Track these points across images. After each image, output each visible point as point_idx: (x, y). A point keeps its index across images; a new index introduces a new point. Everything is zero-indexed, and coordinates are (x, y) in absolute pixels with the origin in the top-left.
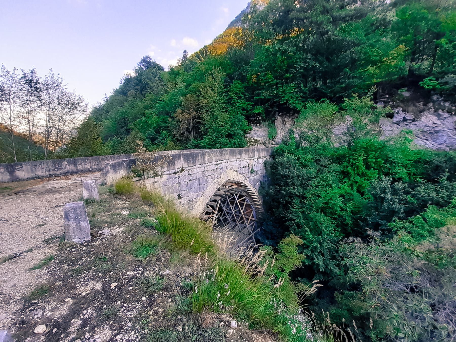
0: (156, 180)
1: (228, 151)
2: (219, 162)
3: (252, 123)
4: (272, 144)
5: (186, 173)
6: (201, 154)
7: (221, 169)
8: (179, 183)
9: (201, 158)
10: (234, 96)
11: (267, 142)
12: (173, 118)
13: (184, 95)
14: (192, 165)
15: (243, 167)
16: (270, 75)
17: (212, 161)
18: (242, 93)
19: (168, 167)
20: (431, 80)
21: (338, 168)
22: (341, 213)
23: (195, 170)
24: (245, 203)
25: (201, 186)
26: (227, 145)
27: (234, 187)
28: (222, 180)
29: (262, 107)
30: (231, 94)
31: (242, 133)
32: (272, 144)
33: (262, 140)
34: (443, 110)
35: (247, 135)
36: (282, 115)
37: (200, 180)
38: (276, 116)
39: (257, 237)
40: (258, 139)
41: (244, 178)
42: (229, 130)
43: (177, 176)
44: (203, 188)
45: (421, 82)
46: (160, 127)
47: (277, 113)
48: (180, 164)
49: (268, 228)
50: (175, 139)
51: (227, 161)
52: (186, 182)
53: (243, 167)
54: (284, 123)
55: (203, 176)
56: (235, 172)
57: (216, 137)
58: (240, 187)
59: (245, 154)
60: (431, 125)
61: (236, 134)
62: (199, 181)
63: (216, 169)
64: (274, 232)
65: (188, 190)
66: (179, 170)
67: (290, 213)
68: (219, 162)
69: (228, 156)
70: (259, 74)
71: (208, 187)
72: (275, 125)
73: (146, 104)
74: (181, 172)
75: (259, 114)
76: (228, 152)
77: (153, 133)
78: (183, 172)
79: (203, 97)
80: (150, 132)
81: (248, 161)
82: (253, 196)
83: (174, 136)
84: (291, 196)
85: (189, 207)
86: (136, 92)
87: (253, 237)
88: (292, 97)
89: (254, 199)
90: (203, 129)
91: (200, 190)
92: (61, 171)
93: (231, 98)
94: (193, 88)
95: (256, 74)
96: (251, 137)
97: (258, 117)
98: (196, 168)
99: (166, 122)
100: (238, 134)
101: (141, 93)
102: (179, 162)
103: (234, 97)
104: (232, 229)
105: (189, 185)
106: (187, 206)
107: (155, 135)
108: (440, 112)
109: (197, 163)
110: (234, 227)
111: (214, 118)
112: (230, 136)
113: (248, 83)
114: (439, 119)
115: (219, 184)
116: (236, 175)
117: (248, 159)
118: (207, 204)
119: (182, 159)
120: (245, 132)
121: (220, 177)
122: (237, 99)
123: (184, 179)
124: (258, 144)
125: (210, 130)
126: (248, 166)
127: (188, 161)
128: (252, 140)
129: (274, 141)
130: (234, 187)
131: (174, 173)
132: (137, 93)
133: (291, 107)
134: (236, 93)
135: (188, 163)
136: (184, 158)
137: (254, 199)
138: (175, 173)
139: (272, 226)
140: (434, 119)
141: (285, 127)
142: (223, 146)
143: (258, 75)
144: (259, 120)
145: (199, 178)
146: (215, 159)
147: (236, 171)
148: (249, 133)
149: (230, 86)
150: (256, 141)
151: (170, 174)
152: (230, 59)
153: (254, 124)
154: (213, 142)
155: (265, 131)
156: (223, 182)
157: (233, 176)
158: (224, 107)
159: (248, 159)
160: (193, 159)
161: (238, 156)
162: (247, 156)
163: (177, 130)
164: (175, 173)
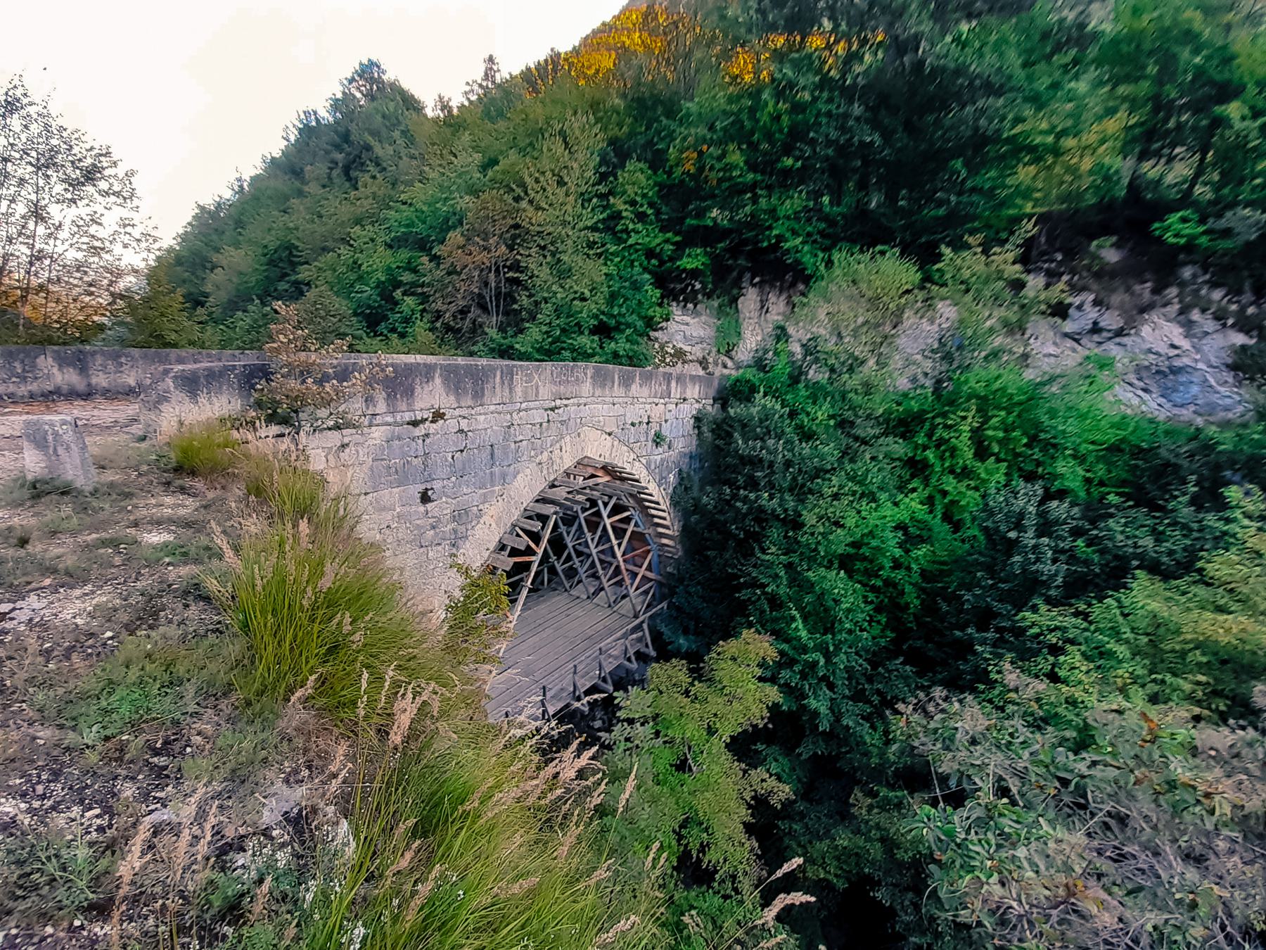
2: (558, 402)
4: (725, 366)
5: (452, 425)
11: (711, 360)
12: (435, 258)
13: (474, 191)
14: (470, 403)
18: (651, 205)
19: (391, 397)
20: (1184, 220)
21: (899, 448)
24: (631, 528)
25: (496, 470)
26: (593, 355)
27: (599, 480)
29: (706, 253)
30: (618, 203)
32: (725, 366)
33: (697, 351)
34: (1203, 311)
40: (687, 348)
41: (633, 456)
42: (603, 313)
44: (504, 476)
45: (1157, 225)
46: (398, 285)
47: (748, 276)
48: (432, 395)
51: (582, 401)
53: (633, 424)
54: (763, 307)
57: (563, 331)
60: (1163, 348)
62: (492, 455)
65: (453, 479)
68: (558, 402)
69: (587, 388)
75: (695, 274)
78: (441, 422)
81: (648, 407)
82: (653, 512)
84: (761, 516)
85: (455, 531)
87: (645, 626)
90: (525, 301)
92: (34, 387)
93: (617, 216)
96: (666, 339)
99: (415, 271)
100: (628, 326)
102: (427, 388)
103: (624, 214)
105: (459, 465)
108: (1195, 315)
109: (486, 399)
110: (596, 593)
111: (563, 273)
112: (603, 330)
113: (670, 173)
119: (438, 381)
120: (650, 324)
124: (684, 362)
125: (547, 308)
127: (457, 389)
128: (669, 350)
129: (731, 358)
130: (599, 480)
131: (408, 424)
134: (633, 203)
136: (446, 380)
138: (415, 423)
140: (1175, 333)
142: (581, 355)
143: (701, 153)
144: (695, 292)
146: (545, 391)
147: (610, 434)
148: (661, 329)
150: (679, 354)
151: (396, 424)
152: (624, 96)
153: (678, 302)
156: (568, 462)
157: (599, 448)
161: (618, 390)
162: (645, 391)
163: (449, 299)
164: (415, 423)
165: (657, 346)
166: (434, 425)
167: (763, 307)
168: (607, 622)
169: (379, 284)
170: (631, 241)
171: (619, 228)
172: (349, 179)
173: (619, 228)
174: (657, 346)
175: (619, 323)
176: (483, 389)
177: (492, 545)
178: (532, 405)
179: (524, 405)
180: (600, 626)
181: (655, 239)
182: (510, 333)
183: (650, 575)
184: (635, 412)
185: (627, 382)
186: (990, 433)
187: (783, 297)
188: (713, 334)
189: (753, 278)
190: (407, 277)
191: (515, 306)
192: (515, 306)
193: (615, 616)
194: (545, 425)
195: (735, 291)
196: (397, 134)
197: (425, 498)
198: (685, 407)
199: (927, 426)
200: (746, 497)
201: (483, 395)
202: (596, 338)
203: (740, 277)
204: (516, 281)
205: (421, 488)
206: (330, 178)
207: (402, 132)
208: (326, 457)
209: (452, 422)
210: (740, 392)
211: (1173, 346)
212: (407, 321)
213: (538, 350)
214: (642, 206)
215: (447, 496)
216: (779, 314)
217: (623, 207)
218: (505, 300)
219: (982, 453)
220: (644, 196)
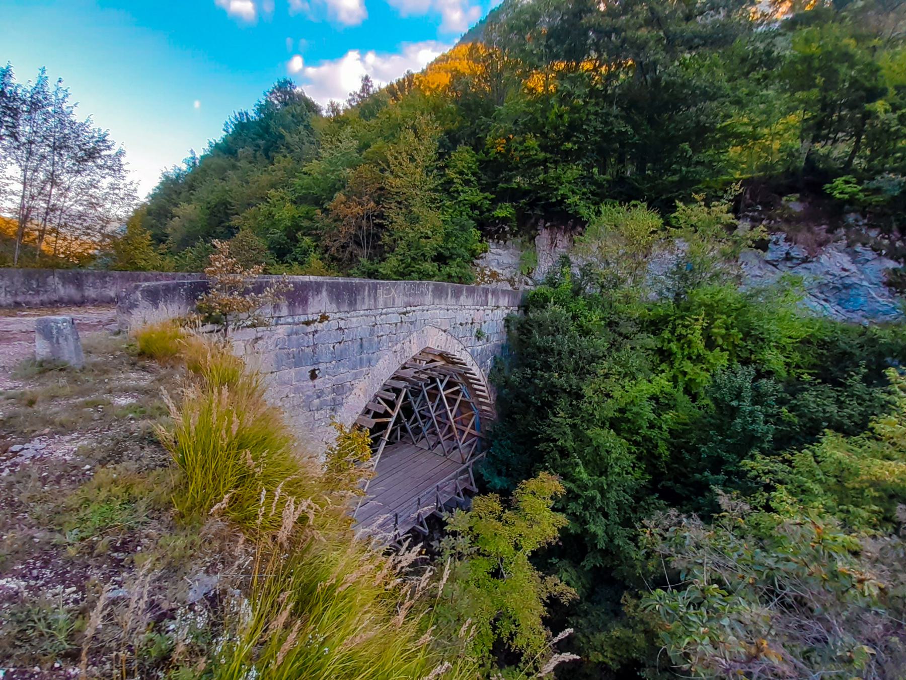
0: (259, 335)
2: (408, 309)
4: (527, 284)
5: (334, 324)
7: (412, 323)
8: (315, 345)
9: (369, 295)
11: (516, 279)
12: (325, 211)
14: (346, 309)
15: (461, 324)
18: (474, 174)
19: (291, 305)
20: (847, 182)
23: (354, 320)
24: (460, 398)
25: (364, 356)
27: (437, 364)
30: (451, 173)
31: (467, 255)
32: (527, 284)
33: (507, 273)
34: (864, 245)
35: (478, 261)
40: (500, 271)
42: (441, 247)
43: (311, 328)
45: (828, 186)
46: (299, 228)
48: (320, 304)
51: (426, 307)
53: (461, 324)
54: (553, 243)
55: (372, 333)
57: (413, 259)
60: (837, 272)
65: (334, 362)
68: (408, 309)
69: (429, 298)
70: (511, 136)
75: (505, 220)
78: (326, 322)
81: (472, 312)
87: (470, 469)
88: (573, 192)
90: (387, 239)
93: (450, 182)
94: (373, 153)
99: (311, 219)
100: (459, 256)
102: (317, 299)
105: (338, 352)
107: (286, 243)
108: (859, 248)
109: (358, 306)
111: (414, 220)
112: (441, 259)
113: (487, 153)
114: (854, 262)
117: (473, 307)
120: (474, 254)
121: (408, 339)
125: (402, 244)
128: (487, 272)
130: (437, 364)
131: (303, 323)
132: (258, 154)
134: (461, 173)
138: (307, 323)
143: (508, 140)
147: (445, 331)
148: (482, 258)
149: (450, 157)
150: (494, 275)
153: (493, 239)
156: (415, 351)
157: (437, 341)
158: (436, 199)
162: (470, 301)
164: (307, 323)
165: (478, 269)
166: (321, 325)
169: (286, 228)
172: (268, 157)
174: (478, 269)
175: (452, 254)
177: (360, 411)
178: (389, 310)
179: (384, 311)
182: (376, 260)
185: (457, 294)
187: (568, 235)
189: (545, 223)
196: (301, 127)
197: (313, 376)
202: (436, 264)
203: (536, 223)
206: (255, 157)
211: (844, 270)
212: (305, 253)
213: (395, 273)
217: (454, 176)
219: (710, 344)
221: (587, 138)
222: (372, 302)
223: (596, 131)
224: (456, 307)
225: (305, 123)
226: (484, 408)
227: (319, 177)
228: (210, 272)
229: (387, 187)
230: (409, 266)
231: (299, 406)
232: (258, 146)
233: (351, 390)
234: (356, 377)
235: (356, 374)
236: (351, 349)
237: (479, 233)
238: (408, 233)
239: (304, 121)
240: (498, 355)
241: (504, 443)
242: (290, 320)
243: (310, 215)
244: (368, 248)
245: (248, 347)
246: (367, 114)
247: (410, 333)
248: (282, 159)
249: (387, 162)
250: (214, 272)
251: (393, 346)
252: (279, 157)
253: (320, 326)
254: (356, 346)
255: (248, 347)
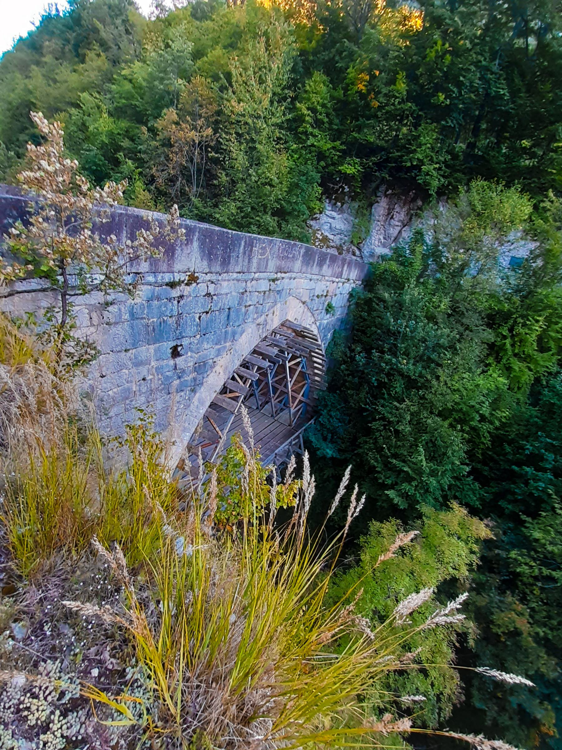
0: (110, 298)
1: (303, 251)
3: (327, 198)
4: (354, 254)
5: (202, 288)
6: (245, 242)
7: (279, 292)
8: (180, 314)
9: (244, 253)
10: (309, 115)
11: (345, 248)
12: (152, 130)
14: (218, 269)
16: (402, 86)
17: (266, 268)
18: (328, 115)
21: (489, 335)
22: (480, 426)
23: (225, 284)
24: (299, 369)
25: (230, 329)
28: (275, 319)
29: (361, 164)
30: (302, 107)
32: (354, 254)
33: (336, 240)
35: (312, 223)
36: (392, 194)
37: (231, 313)
38: (379, 194)
39: (308, 437)
40: (331, 237)
43: (176, 293)
44: (234, 334)
46: (119, 148)
47: (383, 188)
49: (330, 422)
50: (152, 188)
51: (294, 275)
52: (198, 315)
54: (389, 215)
55: (239, 304)
56: (301, 304)
57: (253, 208)
58: (300, 338)
59: (329, 266)
61: (296, 213)
62: (228, 316)
63: (270, 290)
64: (341, 431)
65: (198, 337)
66: (185, 277)
67: (382, 406)
68: (279, 275)
69: (298, 264)
70: (377, 73)
71: (244, 332)
72: (371, 214)
73: (86, 80)
74: (187, 284)
76: (301, 254)
77: (100, 160)
78: (194, 285)
79: (234, 93)
80: (92, 153)
82: (315, 359)
83: (152, 180)
84: (392, 373)
85: (195, 379)
86: (63, 45)
87: (301, 436)
88: (431, 160)
89: (316, 365)
90: (224, 178)
91: (226, 338)
93: (299, 119)
94: (211, 64)
95: (370, 71)
97: (341, 187)
98: (229, 280)
101: (76, 51)
103: (307, 118)
104: (257, 408)
105: (203, 324)
106: (191, 376)
107: (104, 165)
109: (231, 268)
110: (263, 406)
113: (346, 90)
115: (268, 327)
116: (302, 311)
117: (331, 279)
118: (234, 372)
119: (196, 244)
121: (271, 311)
122: (312, 126)
123: (193, 305)
125: (242, 187)
126: (326, 296)
127: (210, 254)
128: (319, 236)
129: (359, 249)
131: (167, 284)
132: (67, 49)
133: (419, 181)
134: (313, 110)
135: (210, 260)
136: (202, 244)
137: (316, 365)
138: (172, 285)
139: (338, 419)
141: (390, 224)
143: (373, 77)
145: (229, 309)
146: (272, 265)
147: (304, 303)
148: (316, 219)
149: (304, 86)
150: (325, 239)
153: (330, 200)
154: (243, 218)
155: (348, 223)
156: (275, 323)
159: (331, 279)
160: (225, 251)
161: (315, 269)
164: (172, 285)
166: (188, 288)
167: (389, 215)
168: (272, 427)
169: (103, 146)
170: (309, 143)
171: (301, 129)
172: (78, 55)
173: (301, 129)
175: (294, 210)
176: (229, 257)
177: (219, 388)
178: (262, 275)
179: (257, 275)
180: (267, 431)
181: (326, 145)
183: (303, 399)
184: (320, 287)
186: (553, 334)
187: (407, 207)
188: (350, 228)
189: (387, 190)
190: (126, 143)
191: (215, 182)
192: (215, 182)
193: (276, 424)
194: (267, 293)
195: (373, 198)
196: (119, 21)
197: (175, 353)
198: (347, 285)
199: (511, 322)
200: (390, 360)
201: (229, 263)
202: (276, 218)
203: (377, 188)
204: (216, 161)
205: (172, 344)
206: (63, 53)
207: (123, 21)
208: (89, 314)
209: (202, 286)
210: (385, 279)
213: (232, 222)
214: (320, 114)
215: (192, 351)
216: (399, 221)
217: (306, 112)
218: (205, 175)
219: (543, 348)
220: (323, 106)
221: (460, 94)
222: (246, 263)
223: (472, 86)
224: (318, 277)
225: (124, 18)
226: (317, 378)
227: (144, 84)
228: (28, 181)
229: (227, 112)
230: (247, 216)
231: (157, 389)
232: (68, 41)
233: (212, 367)
234: (219, 353)
235: (219, 350)
236: (218, 321)
237: (320, 190)
238: (250, 175)
239: (121, 14)
240: (337, 328)
241: (333, 414)
242: (151, 279)
243: (131, 134)
244: (198, 187)
245: (94, 315)
246: (199, 14)
247: (275, 303)
248: (95, 57)
249: (228, 76)
250: (39, 183)
251: (258, 318)
252: (91, 55)
253: (187, 290)
254: (224, 316)
255: (94, 315)
